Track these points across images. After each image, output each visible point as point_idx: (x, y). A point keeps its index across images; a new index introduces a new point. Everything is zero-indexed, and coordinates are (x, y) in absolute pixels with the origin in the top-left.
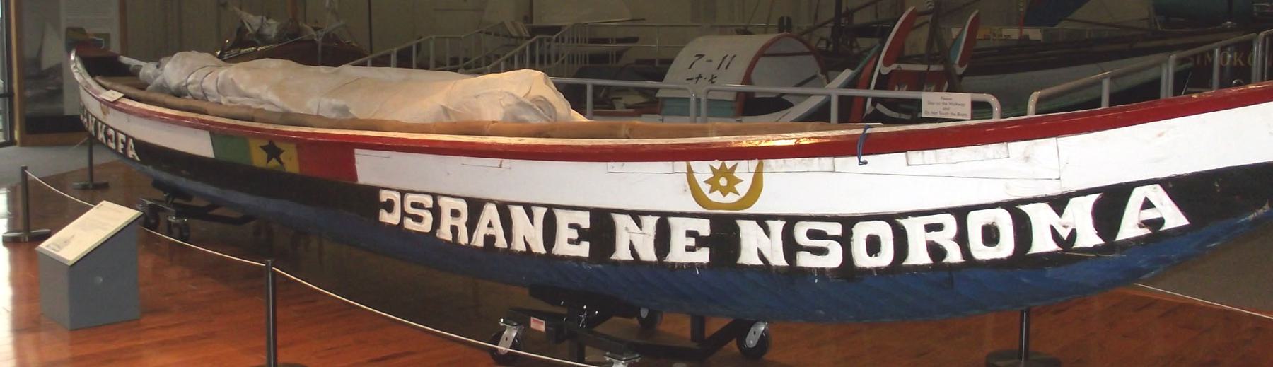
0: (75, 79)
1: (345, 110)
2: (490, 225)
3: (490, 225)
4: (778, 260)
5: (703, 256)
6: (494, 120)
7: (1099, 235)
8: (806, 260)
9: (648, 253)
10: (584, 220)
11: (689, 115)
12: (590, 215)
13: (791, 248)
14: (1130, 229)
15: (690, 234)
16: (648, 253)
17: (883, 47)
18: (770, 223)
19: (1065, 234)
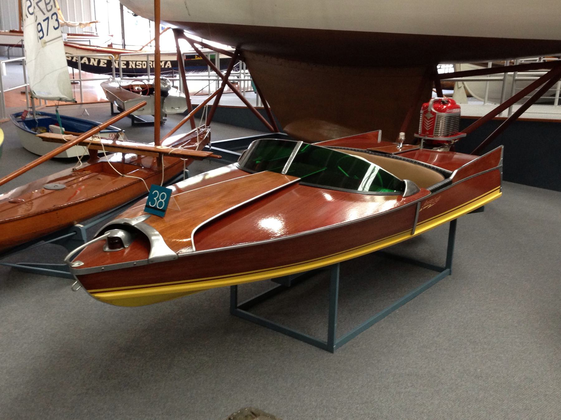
0: (246, 65)
1: (125, 58)
2: (169, 64)
3: (169, 64)
4: (134, 67)
5: (105, 66)
6: (26, 51)
7: (107, 98)
8: (137, 67)
9: (96, 64)
10: (125, 62)
11: (220, 59)
12: (452, 73)
13: (136, 65)
14: (166, 67)
15: (123, 63)
16: (96, 64)
17: (26, 262)
18: (133, 62)
19: (104, 63)
